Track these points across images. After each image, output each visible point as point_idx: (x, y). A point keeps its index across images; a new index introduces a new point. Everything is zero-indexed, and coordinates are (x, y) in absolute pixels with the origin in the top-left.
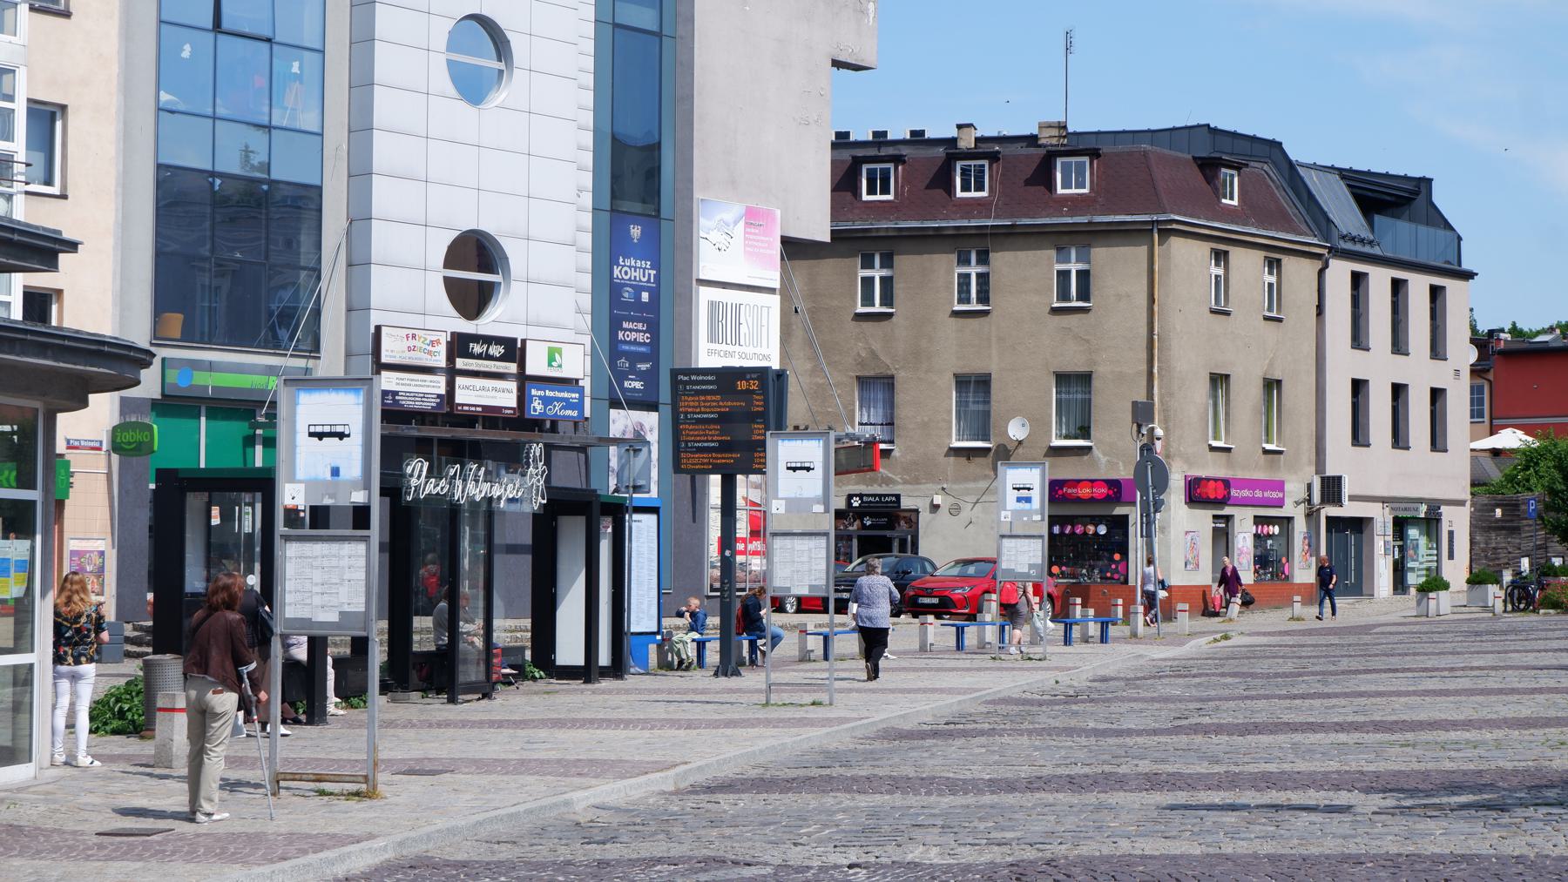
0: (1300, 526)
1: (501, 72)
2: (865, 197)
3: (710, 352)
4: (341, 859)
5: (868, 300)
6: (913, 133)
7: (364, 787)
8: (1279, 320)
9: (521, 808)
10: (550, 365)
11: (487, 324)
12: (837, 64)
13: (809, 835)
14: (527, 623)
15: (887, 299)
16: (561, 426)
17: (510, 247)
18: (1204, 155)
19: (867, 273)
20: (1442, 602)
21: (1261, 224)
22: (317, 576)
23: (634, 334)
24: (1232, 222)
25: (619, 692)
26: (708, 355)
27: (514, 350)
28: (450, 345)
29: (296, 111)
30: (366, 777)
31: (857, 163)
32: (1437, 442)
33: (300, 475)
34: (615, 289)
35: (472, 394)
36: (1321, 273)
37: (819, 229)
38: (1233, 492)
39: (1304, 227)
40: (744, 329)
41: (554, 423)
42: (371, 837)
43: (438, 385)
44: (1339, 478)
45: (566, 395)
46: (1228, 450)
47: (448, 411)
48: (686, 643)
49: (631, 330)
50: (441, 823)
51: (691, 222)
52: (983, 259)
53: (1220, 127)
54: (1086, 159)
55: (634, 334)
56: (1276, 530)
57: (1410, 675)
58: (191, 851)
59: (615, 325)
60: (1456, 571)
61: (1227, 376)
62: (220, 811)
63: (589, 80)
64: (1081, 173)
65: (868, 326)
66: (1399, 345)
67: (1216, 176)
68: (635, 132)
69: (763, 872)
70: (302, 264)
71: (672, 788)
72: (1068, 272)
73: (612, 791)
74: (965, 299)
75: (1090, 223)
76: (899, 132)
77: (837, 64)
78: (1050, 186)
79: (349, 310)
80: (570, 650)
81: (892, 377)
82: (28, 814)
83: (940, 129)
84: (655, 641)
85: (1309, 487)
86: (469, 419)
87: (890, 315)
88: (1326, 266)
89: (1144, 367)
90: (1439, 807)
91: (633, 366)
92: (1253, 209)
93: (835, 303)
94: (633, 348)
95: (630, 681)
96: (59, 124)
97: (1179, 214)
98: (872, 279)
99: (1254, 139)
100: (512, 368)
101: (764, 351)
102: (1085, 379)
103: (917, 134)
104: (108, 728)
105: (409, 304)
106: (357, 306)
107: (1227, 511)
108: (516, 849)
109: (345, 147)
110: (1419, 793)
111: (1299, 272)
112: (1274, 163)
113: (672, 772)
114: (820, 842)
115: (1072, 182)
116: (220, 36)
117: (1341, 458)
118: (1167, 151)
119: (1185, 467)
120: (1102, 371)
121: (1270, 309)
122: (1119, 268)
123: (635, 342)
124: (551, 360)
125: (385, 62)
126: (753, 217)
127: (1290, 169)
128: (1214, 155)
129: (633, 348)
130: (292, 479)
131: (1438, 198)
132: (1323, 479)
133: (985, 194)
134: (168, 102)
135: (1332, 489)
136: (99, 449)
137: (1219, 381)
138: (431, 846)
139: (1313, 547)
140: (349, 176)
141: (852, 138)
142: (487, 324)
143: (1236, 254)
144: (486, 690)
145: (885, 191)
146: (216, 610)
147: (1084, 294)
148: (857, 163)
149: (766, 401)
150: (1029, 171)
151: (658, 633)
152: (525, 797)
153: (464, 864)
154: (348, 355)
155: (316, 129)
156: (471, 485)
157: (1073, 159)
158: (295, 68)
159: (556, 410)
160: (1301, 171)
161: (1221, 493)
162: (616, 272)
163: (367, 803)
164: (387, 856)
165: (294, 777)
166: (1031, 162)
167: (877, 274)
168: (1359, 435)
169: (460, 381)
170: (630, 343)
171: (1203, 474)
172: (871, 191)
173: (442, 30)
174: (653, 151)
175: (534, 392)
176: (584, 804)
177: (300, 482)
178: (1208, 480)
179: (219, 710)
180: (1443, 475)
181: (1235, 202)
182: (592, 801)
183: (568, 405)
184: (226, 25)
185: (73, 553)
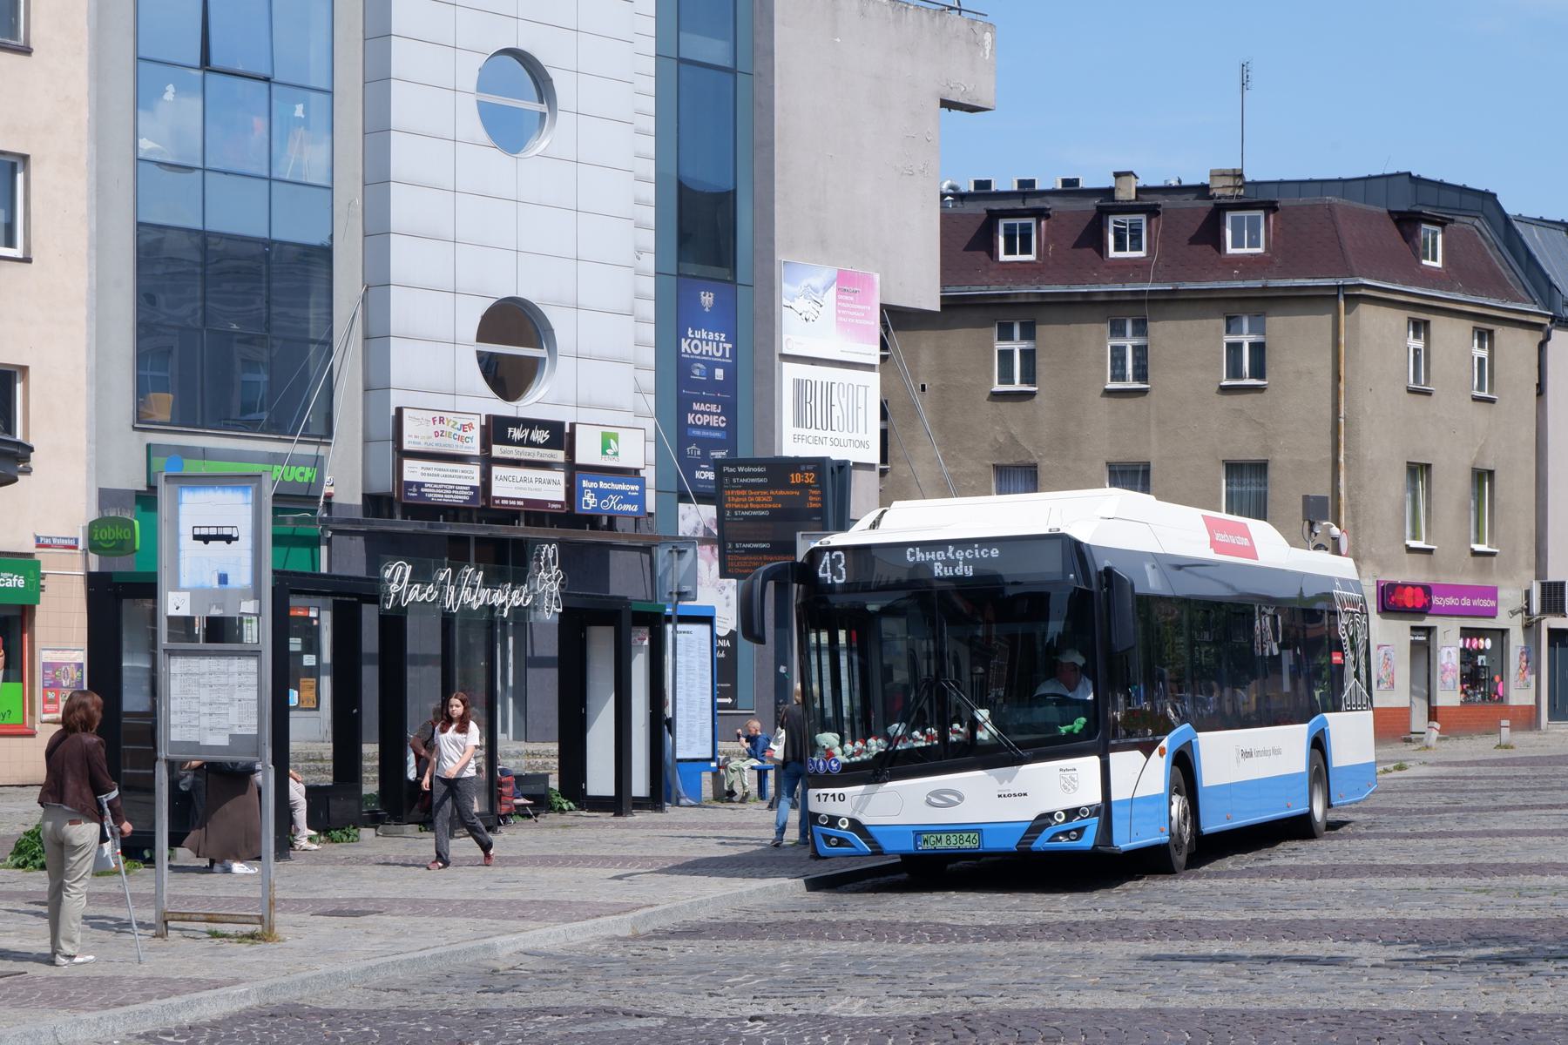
0: (1517, 640)
1: (543, 115)
2: (1003, 257)
3: (796, 438)
4: (189, 1006)
5: (1007, 377)
6: (1066, 182)
7: (259, 928)
8: (1492, 401)
9: (428, 953)
10: (604, 453)
12: (946, 104)
13: (732, 985)
14: (554, 748)
15: (1029, 376)
16: (619, 524)
17: (554, 316)
18: (1405, 209)
19: (1006, 345)
21: (1470, 288)
22: (205, 695)
23: (707, 416)
24: (1434, 287)
25: (656, 826)
27: (561, 436)
28: (485, 431)
29: (304, 158)
30: (261, 918)
33: (185, 582)
34: (683, 366)
35: (511, 486)
36: (1542, 346)
37: (926, 296)
38: (1436, 601)
39: (1521, 293)
40: (836, 411)
41: (611, 520)
42: (236, 981)
43: (470, 475)
44: (1563, 584)
45: (623, 487)
46: (1430, 551)
47: (483, 506)
48: (744, 773)
49: (703, 413)
50: (323, 968)
51: (773, 288)
53: (1424, 175)
54: (1261, 214)
55: (707, 416)
56: (1488, 644)
57: (1557, 811)
58: (67, 995)
59: (684, 407)
61: (1428, 466)
62: (85, 951)
63: (650, 124)
64: (1254, 230)
65: (1006, 407)
67: (1415, 233)
69: (652, 1024)
70: (312, 336)
71: (628, 933)
72: (1239, 346)
73: (550, 936)
74: (1119, 375)
75: (1265, 288)
76: (1048, 181)
77: (946, 104)
78: (1218, 244)
79: (366, 389)
80: (600, 780)
81: (1035, 466)
83: (1094, 177)
84: (710, 769)
85: (1528, 594)
86: (508, 515)
87: (1033, 394)
88: (1548, 338)
89: (1329, 455)
90: (1451, 961)
91: (705, 455)
92: (1460, 271)
93: (968, 380)
94: (705, 433)
95: (672, 813)
96: (20, 177)
97: (1369, 278)
98: (1124, 348)
99: (1463, 190)
100: (559, 456)
101: (861, 436)
103: (1070, 183)
104: (37, 862)
105: (434, 388)
106: (376, 384)
107: (1428, 622)
108: (406, 998)
109: (359, 202)
110: (1432, 946)
111: (1515, 345)
112: (1487, 218)
113: (630, 916)
114: (741, 993)
115: (1242, 241)
116: (209, 76)
118: (1356, 205)
119: (1378, 572)
120: (1280, 461)
121: (1481, 388)
122: (1298, 340)
123: (708, 427)
124: (605, 447)
125: (404, 103)
126: (846, 282)
127: (1506, 227)
128: (1414, 208)
129: (705, 433)
130: (176, 587)
132: (1543, 585)
133: (1142, 254)
134: (151, 151)
136: (75, 547)
137: (1418, 471)
138: (306, 992)
139: (1532, 664)
140: (365, 236)
141: (1037, 187)
143: (1438, 324)
145: (1026, 249)
146: (74, 730)
147: (1258, 370)
148: (993, 216)
149: (823, 496)
150: (1194, 227)
151: (713, 759)
153: (332, 1013)
154: (366, 441)
155: (326, 183)
156: (465, 593)
157: (1246, 214)
158: (299, 111)
159: (612, 504)
160: (1518, 226)
161: (1420, 600)
162: (685, 345)
163: (262, 945)
164: (248, 1004)
165: (184, 917)
167: (1017, 346)
169: (497, 471)
170: (702, 427)
171: (1399, 578)
172: (1010, 250)
173: (470, 68)
174: (725, 202)
175: (585, 483)
176: (511, 949)
177: (184, 590)
178: (1405, 586)
179: (77, 842)
181: (1438, 264)
182: (521, 947)
183: (626, 498)
184: (215, 61)
185: (46, 665)
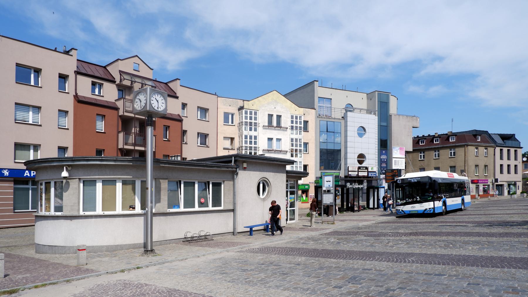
0: (491, 186)
5: (421, 158)
11: (363, 165)
15: (424, 158)
17: (366, 155)
20: (515, 196)
26: (394, 167)
27: (367, 168)
31: (419, 140)
32: (516, 172)
34: (381, 159)
35: (361, 174)
43: (356, 173)
47: (358, 176)
52: (438, 151)
55: (384, 165)
59: (381, 164)
60: (519, 192)
66: (509, 158)
68: (384, 138)
76: (426, 135)
78: (449, 140)
80: (371, 206)
82: (293, 226)
83: (432, 134)
86: (361, 177)
92: (482, 141)
102: (455, 167)
105: (352, 164)
106: (346, 164)
111: (491, 150)
117: (498, 175)
120: (457, 166)
122: (460, 151)
125: (349, 133)
126: (401, 149)
127: (489, 135)
128: (475, 134)
131: (516, 137)
135: (496, 180)
142: (363, 165)
143: (480, 148)
144: (359, 211)
152: (354, 224)
166: (445, 138)
167: (422, 155)
168: (501, 172)
174: (386, 141)
180: (518, 178)
